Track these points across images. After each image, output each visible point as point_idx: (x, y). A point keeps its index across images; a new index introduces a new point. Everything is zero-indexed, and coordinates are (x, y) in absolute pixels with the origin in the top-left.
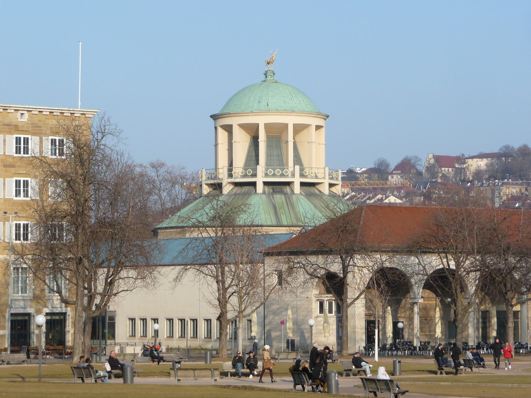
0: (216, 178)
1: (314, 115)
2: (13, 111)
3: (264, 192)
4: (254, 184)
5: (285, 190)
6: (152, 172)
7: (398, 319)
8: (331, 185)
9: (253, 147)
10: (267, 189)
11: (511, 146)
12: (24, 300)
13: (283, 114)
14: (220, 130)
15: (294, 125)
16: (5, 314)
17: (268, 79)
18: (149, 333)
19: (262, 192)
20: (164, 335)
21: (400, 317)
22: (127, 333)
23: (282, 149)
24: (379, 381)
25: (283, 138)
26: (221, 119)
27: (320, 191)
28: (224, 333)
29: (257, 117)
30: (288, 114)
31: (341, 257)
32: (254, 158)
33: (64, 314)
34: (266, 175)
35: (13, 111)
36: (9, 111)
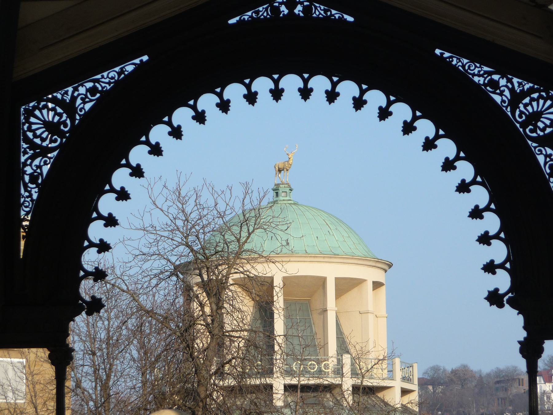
3: (287, 405)
11: (442, 368)
15: (336, 279)
17: (281, 198)
23: (313, 326)
25: (316, 305)
27: (383, 401)
30: (326, 260)
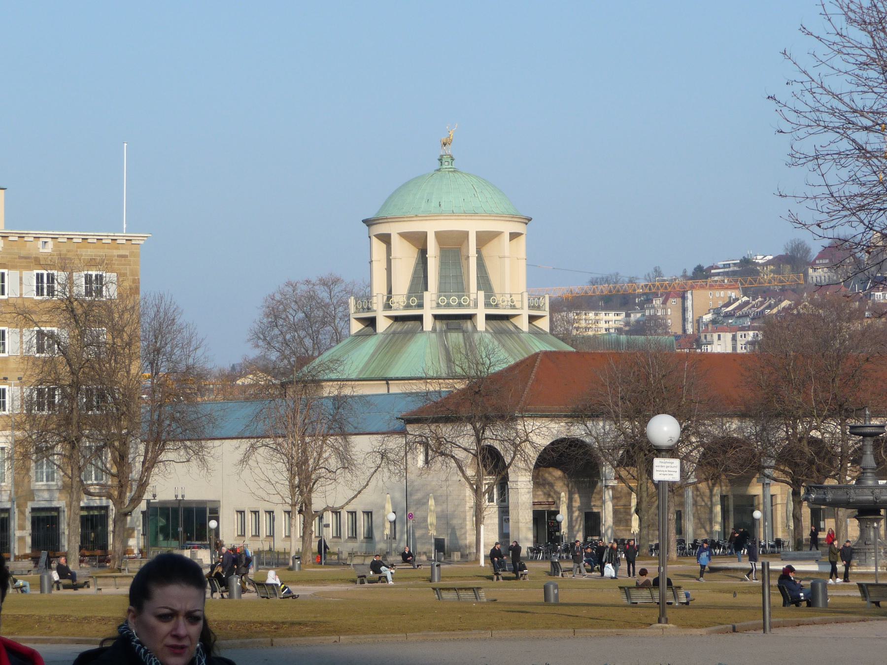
0: (369, 309)
1: (507, 219)
2: (32, 239)
3: (434, 330)
4: (419, 318)
5: (465, 326)
6: (322, 292)
7: (592, 509)
8: (532, 318)
9: (421, 265)
10: (438, 324)
12: (49, 490)
13: (468, 218)
14: (375, 240)
15: (477, 232)
16: (25, 510)
17: (444, 167)
18: (263, 531)
19: (430, 330)
20: (282, 533)
21: (594, 506)
22: (234, 531)
24: (268, 585)
26: (375, 226)
27: (516, 327)
28: (308, 532)
29: (424, 222)
31: (474, 428)
32: (422, 280)
33: (106, 508)
34: (438, 306)
35: (32, 239)
36: (26, 239)
